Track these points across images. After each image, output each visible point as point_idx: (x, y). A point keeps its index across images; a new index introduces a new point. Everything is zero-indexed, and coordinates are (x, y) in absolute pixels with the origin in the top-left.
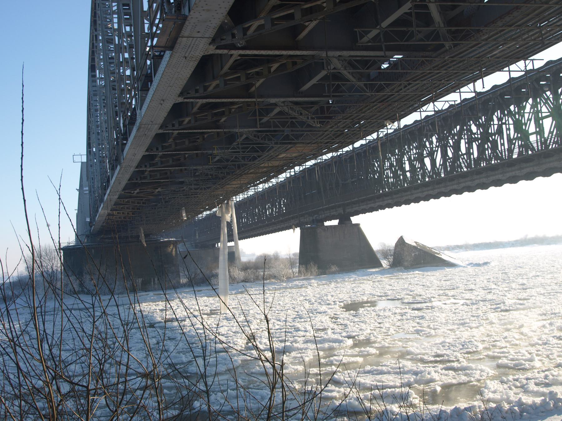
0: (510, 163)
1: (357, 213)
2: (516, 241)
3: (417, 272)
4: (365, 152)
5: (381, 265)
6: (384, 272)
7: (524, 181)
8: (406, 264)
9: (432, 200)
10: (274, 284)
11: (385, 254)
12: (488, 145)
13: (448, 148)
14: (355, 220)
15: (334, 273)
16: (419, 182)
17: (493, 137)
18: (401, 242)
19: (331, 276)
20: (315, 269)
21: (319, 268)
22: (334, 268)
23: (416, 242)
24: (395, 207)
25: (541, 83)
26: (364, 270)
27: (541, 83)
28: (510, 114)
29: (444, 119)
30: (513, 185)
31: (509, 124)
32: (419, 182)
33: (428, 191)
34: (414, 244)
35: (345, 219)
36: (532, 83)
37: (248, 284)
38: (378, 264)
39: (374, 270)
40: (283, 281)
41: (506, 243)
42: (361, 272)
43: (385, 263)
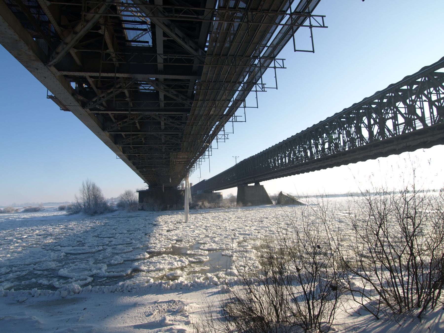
0: (345, 153)
1: (261, 181)
2: (344, 194)
3: (287, 207)
4: (290, 142)
5: (272, 203)
6: (274, 206)
7: (360, 162)
8: (282, 203)
9: (316, 171)
10: (223, 209)
11: (274, 198)
12: (332, 145)
13: (319, 145)
14: (261, 183)
15: (250, 206)
16: (386, 138)
17: (336, 141)
18: (281, 194)
19: (247, 207)
20: (241, 204)
21: (243, 203)
22: (250, 204)
23: (287, 194)
24: (296, 175)
25: (342, 120)
26: (263, 205)
27: (342, 120)
28: (345, 129)
29: (289, 141)
30: (354, 164)
31: (344, 134)
32: (386, 138)
33: (328, 162)
34: (287, 195)
35: (257, 183)
36: (337, 119)
37: (211, 209)
38: (271, 203)
39: (269, 205)
40: (226, 209)
41: (340, 195)
42: (262, 206)
43: (274, 202)
